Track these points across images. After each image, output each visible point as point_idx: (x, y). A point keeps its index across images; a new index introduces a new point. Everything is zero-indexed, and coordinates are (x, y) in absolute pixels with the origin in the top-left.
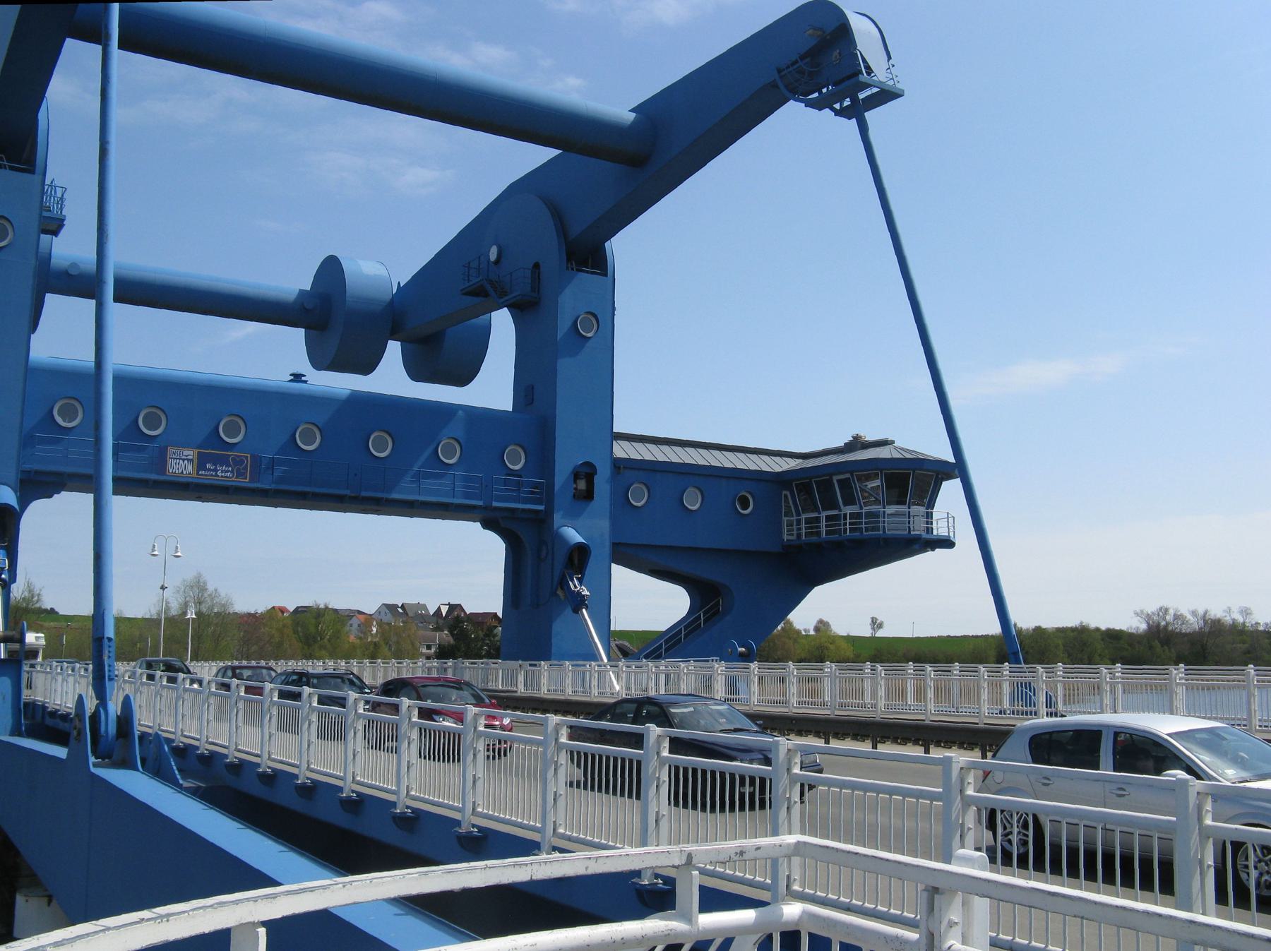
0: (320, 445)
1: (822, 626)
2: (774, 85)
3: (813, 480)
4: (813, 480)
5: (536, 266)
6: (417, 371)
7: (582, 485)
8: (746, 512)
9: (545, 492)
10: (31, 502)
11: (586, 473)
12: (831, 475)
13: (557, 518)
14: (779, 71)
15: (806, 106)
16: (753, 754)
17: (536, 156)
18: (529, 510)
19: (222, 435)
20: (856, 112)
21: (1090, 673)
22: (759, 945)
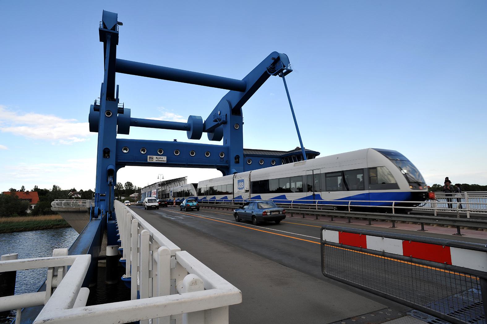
0: (224, 156)
1: (129, 184)
2: (266, 72)
3: (292, 156)
4: (292, 156)
5: (226, 115)
6: (211, 138)
7: (237, 160)
8: (262, 164)
9: (228, 162)
10: (223, 174)
11: (237, 157)
12: (291, 156)
13: (231, 167)
14: (267, 68)
15: (102, 83)
16: (95, 210)
17: (226, 92)
18: (225, 166)
19: (176, 155)
20: (283, 75)
21: (439, 196)
22: (167, 250)
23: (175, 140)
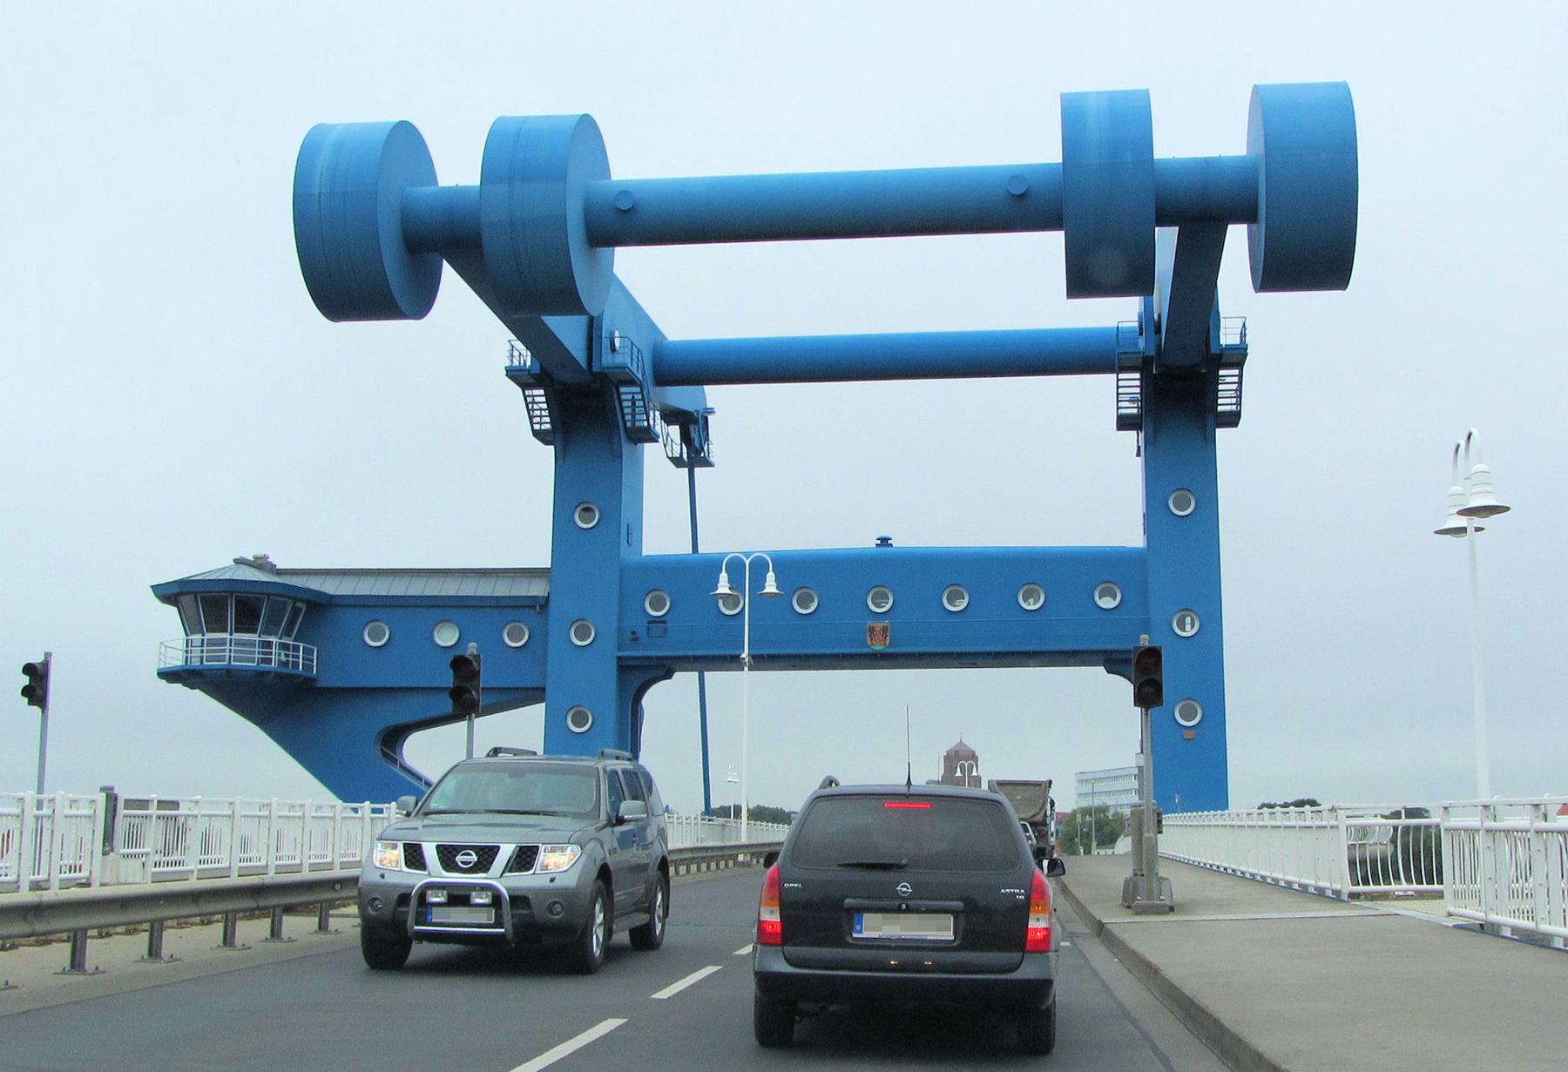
23: (884, 541)
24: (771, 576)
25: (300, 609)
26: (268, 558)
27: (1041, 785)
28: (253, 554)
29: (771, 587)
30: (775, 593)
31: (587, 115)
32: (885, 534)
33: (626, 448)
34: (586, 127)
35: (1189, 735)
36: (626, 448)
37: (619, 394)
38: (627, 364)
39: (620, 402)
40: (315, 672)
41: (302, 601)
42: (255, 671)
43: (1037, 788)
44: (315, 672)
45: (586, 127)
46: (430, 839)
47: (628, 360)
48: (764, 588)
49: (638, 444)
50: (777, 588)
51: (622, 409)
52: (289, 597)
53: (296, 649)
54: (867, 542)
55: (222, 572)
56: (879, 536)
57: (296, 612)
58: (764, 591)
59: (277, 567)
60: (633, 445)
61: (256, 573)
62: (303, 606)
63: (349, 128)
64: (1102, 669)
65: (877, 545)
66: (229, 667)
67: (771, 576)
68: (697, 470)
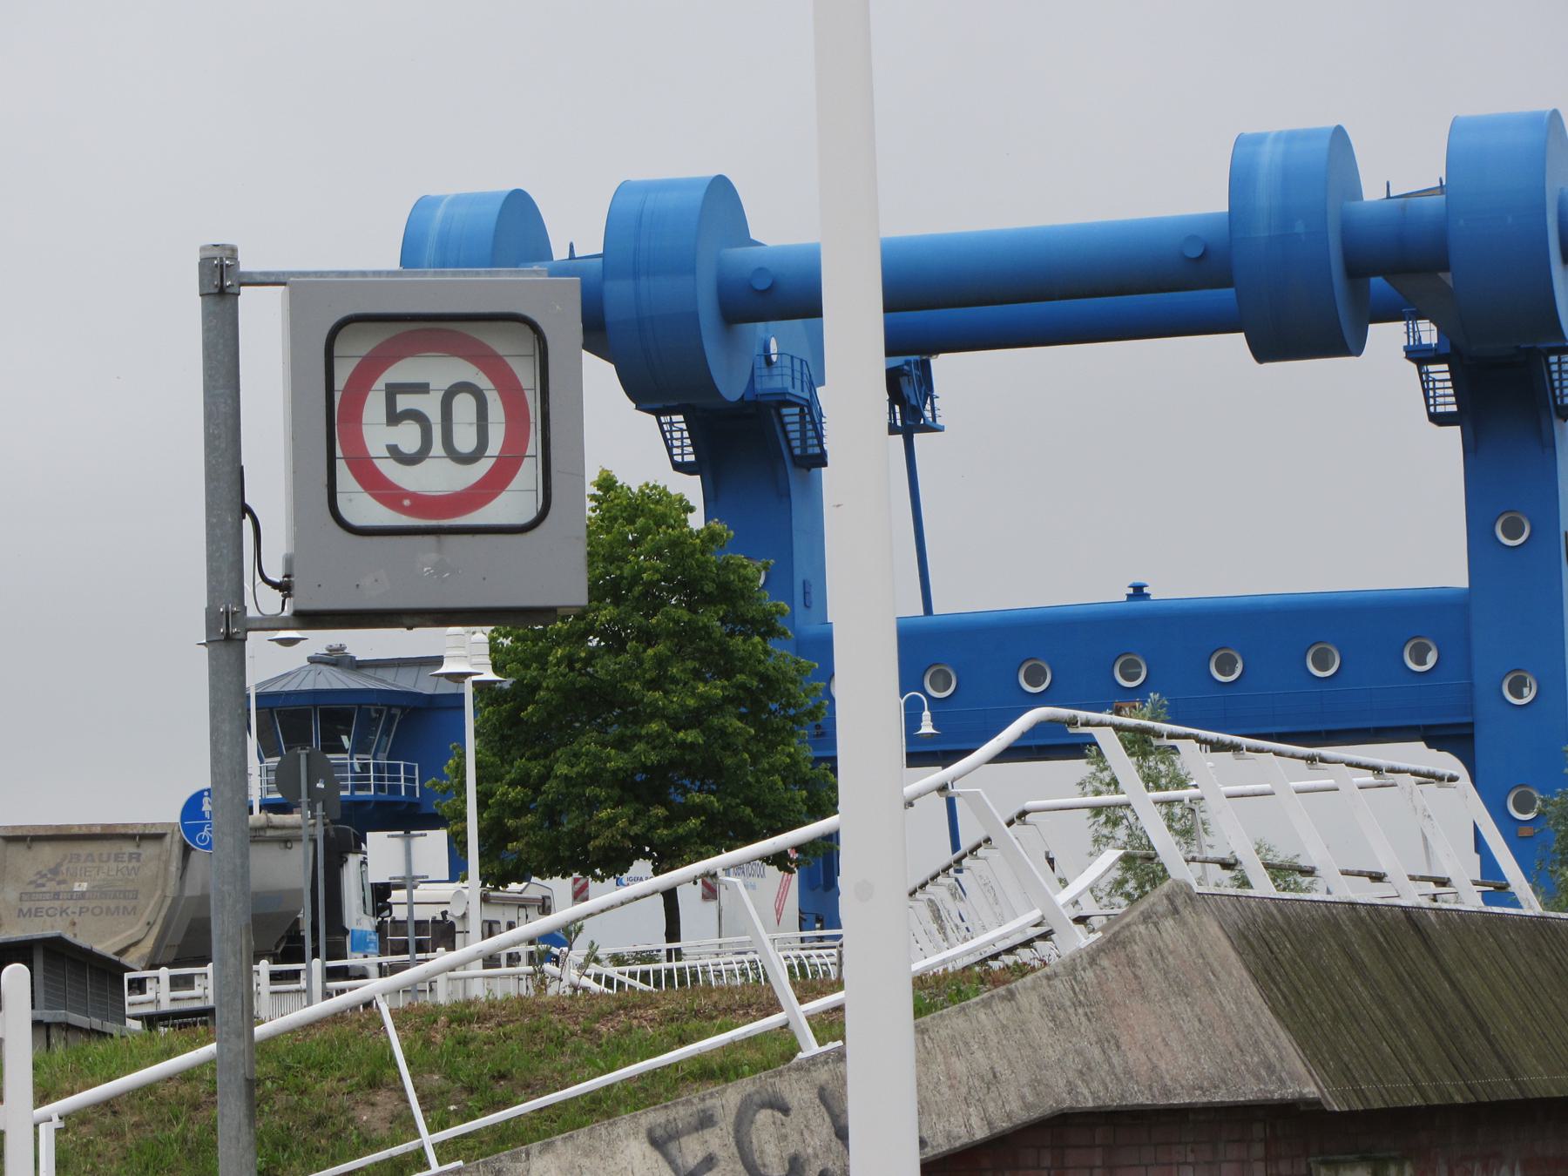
23: (1138, 591)
24: (926, 715)
25: (395, 715)
26: (345, 648)
27: (159, 837)
28: (325, 646)
29: (927, 728)
30: (932, 734)
31: (720, 176)
32: (1138, 580)
33: (794, 476)
34: (721, 191)
35: (1525, 831)
36: (794, 476)
37: (781, 417)
38: (787, 389)
39: (783, 425)
40: (418, 795)
41: (397, 707)
42: (351, 801)
43: (149, 849)
44: (418, 795)
45: (721, 191)
46: (1255, 598)
47: (788, 383)
48: (920, 728)
49: (813, 470)
50: (934, 727)
51: (786, 433)
52: (385, 705)
53: (396, 769)
54: (1115, 593)
55: (286, 680)
56: (1130, 583)
57: (391, 718)
58: (921, 732)
59: (357, 659)
60: (805, 471)
61: (343, 678)
62: (398, 712)
63: (458, 200)
64: (1422, 745)
65: (1129, 596)
66: (377, 799)
67: (926, 715)
68: (918, 438)
